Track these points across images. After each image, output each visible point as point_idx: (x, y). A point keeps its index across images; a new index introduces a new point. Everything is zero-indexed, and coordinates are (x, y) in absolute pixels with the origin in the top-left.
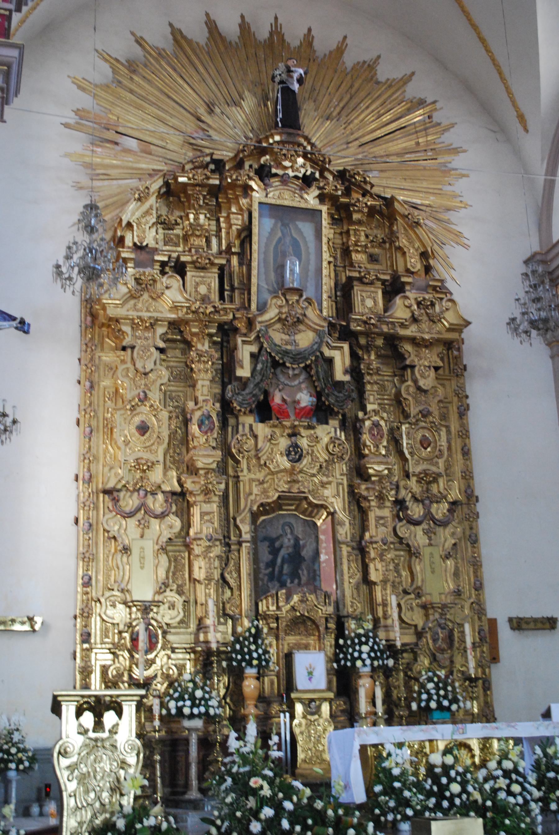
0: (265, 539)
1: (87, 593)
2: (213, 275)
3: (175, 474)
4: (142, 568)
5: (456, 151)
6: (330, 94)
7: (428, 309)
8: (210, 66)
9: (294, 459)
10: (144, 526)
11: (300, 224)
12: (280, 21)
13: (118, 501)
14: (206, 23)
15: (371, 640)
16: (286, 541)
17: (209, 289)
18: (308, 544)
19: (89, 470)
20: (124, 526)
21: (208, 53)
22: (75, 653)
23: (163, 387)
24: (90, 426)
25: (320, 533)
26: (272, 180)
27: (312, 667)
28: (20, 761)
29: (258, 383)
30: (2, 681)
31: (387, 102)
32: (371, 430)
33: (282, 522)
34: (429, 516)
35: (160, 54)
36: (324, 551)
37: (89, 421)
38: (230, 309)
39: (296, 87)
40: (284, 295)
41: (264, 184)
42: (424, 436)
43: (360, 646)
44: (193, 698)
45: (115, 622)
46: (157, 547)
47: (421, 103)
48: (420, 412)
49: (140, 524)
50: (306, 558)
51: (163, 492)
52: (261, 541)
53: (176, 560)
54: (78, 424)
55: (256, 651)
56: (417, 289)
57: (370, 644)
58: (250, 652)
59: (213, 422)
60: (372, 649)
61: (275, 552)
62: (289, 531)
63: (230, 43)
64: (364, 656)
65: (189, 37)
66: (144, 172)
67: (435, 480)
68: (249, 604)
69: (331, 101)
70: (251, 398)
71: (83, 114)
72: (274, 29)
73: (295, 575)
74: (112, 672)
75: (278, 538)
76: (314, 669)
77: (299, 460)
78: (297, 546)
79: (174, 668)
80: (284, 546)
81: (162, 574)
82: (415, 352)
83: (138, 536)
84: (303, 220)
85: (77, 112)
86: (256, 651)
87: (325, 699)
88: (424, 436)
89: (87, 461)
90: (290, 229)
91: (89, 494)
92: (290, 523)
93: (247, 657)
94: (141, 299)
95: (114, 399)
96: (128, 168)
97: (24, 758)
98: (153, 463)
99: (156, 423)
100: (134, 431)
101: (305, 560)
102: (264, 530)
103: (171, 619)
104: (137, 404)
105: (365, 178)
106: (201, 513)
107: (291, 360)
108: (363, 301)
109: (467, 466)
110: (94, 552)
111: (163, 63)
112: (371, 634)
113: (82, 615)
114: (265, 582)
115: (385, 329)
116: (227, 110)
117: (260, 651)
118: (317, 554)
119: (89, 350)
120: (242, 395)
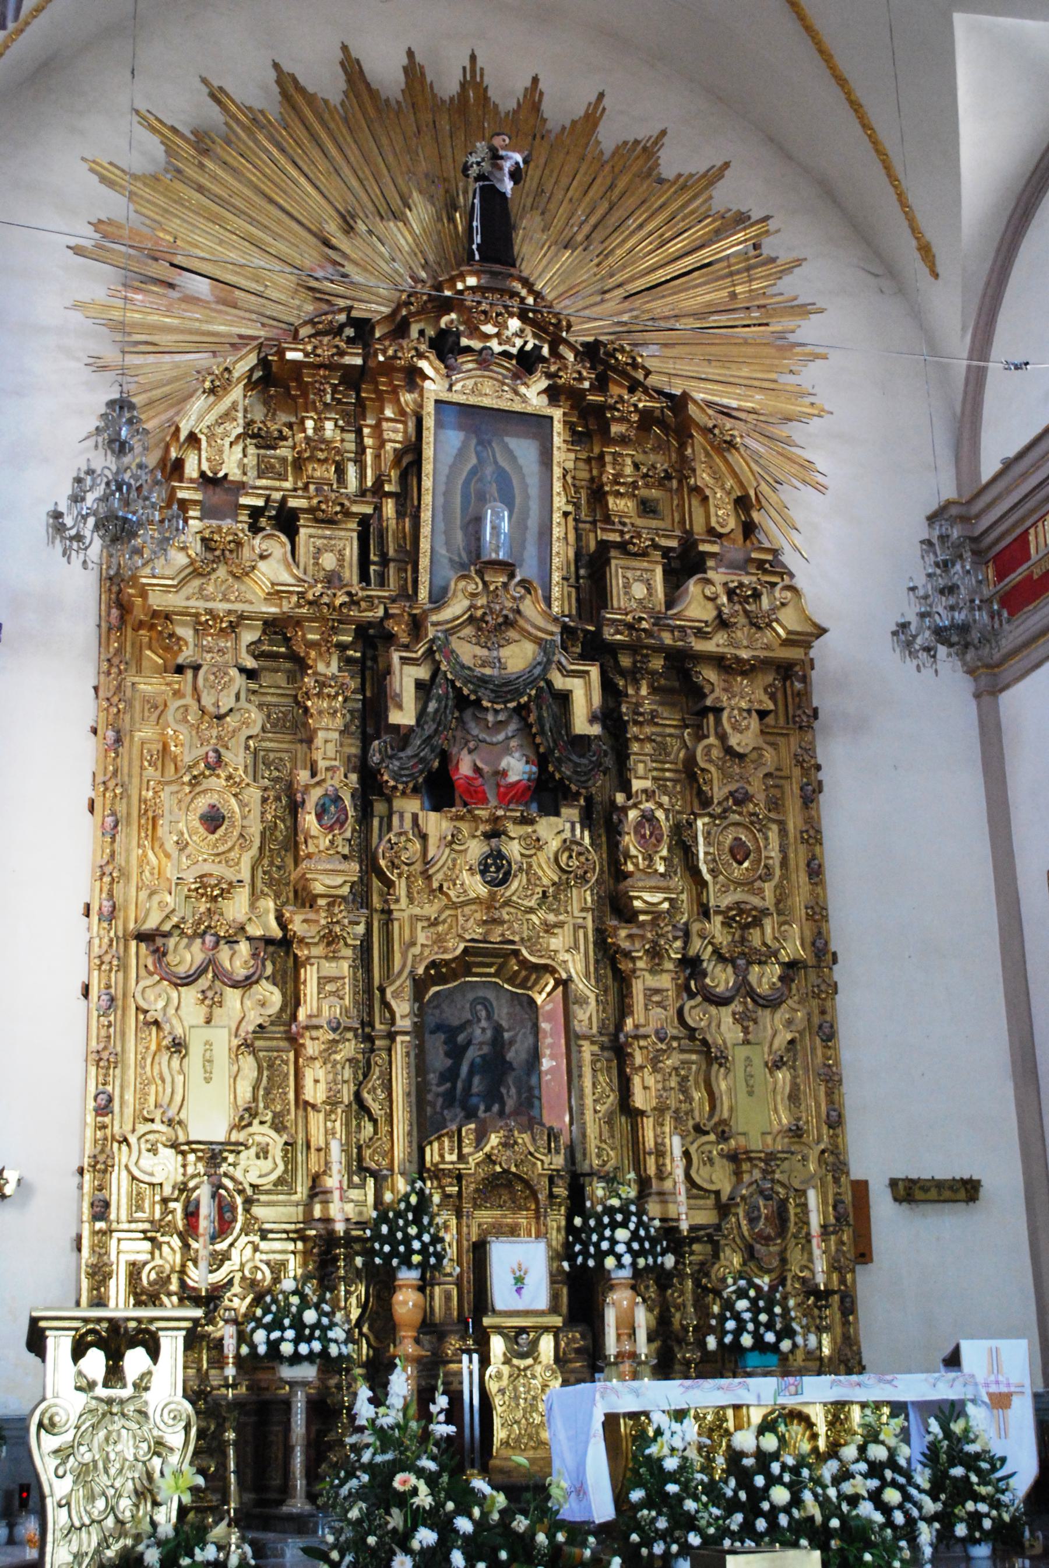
0: (439, 1028)
1: (104, 1127)
4: (208, 1080)
6: (571, 200)
9: (493, 879)
10: (212, 1002)
11: (513, 443)
12: (480, 63)
14: (342, 64)
15: (634, 1219)
17: (341, 560)
18: (519, 1038)
19: (111, 895)
21: (346, 120)
22: (79, 1238)
23: (251, 743)
24: (113, 814)
25: (541, 1019)
27: (523, 1268)
29: (430, 737)
32: (639, 825)
33: (471, 996)
34: (744, 988)
38: (379, 597)
40: (480, 573)
41: (446, 367)
45: (155, 1180)
46: (236, 1042)
47: (741, 220)
48: (731, 794)
50: (515, 1065)
52: (432, 1032)
53: (270, 1066)
54: (92, 809)
56: (727, 567)
57: (632, 1226)
58: (407, 1240)
61: (456, 1052)
62: (483, 1014)
64: (621, 1248)
65: (311, 89)
66: (223, 340)
67: (757, 922)
71: (109, 229)
73: (494, 1096)
74: (147, 1276)
75: (462, 1027)
77: (504, 881)
78: (498, 1043)
81: (245, 1091)
83: (202, 1020)
85: (98, 225)
86: (419, 1237)
87: (546, 1329)
89: (107, 879)
91: (111, 941)
96: (191, 332)
98: (230, 884)
99: (237, 809)
101: (513, 1069)
102: (437, 1012)
105: (634, 359)
106: (319, 978)
110: (119, 1049)
111: (261, 137)
113: (94, 1166)
115: (667, 639)
116: (380, 227)
118: (535, 1057)
119: (114, 670)
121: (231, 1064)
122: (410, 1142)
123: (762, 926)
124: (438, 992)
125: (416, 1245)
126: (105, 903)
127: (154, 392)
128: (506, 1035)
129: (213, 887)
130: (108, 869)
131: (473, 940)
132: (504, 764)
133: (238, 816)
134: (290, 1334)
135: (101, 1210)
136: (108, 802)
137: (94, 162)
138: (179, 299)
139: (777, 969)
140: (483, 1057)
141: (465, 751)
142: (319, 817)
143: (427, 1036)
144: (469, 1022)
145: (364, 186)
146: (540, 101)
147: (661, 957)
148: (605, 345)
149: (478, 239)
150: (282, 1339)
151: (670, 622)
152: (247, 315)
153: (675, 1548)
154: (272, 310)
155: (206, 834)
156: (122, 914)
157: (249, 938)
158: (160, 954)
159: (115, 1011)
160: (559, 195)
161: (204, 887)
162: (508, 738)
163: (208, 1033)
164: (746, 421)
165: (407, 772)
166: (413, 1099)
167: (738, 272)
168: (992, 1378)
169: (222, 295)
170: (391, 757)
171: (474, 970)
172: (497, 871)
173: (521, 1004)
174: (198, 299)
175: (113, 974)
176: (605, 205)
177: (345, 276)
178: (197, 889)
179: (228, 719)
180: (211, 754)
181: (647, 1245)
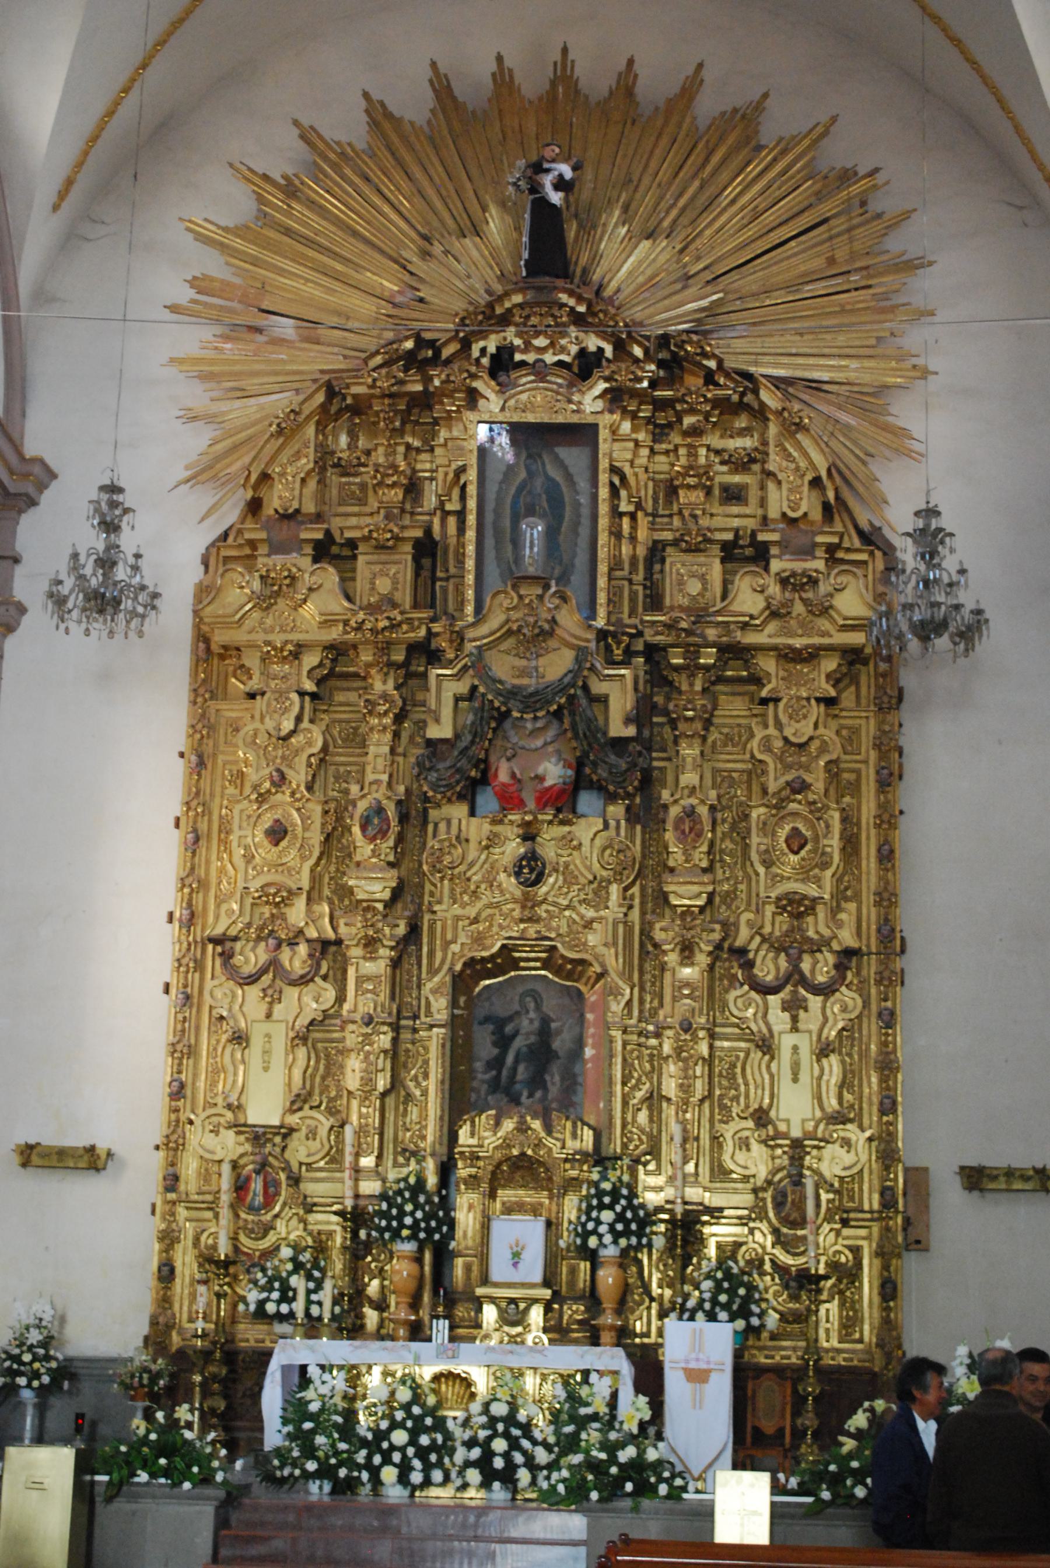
0: (487, 1019)
1: (177, 1110)
2: (404, 557)
3: (327, 909)
4: (266, 1069)
5: (276, 511)
6: (659, 185)
7: (805, 591)
8: (432, 164)
9: (527, 880)
10: (273, 998)
11: (563, 452)
12: (571, 56)
13: (231, 956)
14: (431, 81)
15: (623, 1202)
16: (525, 1023)
17: (395, 582)
18: (566, 1029)
19: (190, 905)
20: (240, 1000)
21: (431, 139)
22: (154, 1206)
23: (313, 760)
24: (195, 830)
25: (587, 1009)
26: (514, 375)
27: (521, 1244)
29: (467, 748)
30: (47, 1248)
31: (775, 186)
32: (679, 821)
33: (520, 989)
34: (795, 977)
35: (343, 154)
36: (590, 1041)
37: (195, 822)
38: (419, 619)
39: (556, 198)
40: (515, 587)
41: (499, 384)
42: (795, 830)
43: (599, 1212)
45: (217, 1158)
46: (292, 1034)
47: (847, 176)
48: (788, 783)
49: (265, 995)
50: (561, 1054)
51: (308, 941)
52: (480, 1023)
53: (328, 1056)
54: (177, 826)
55: (412, 1214)
56: (793, 553)
57: (618, 1208)
58: (402, 1214)
59: (387, 819)
60: (620, 1217)
61: (503, 1042)
62: (532, 1005)
63: (473, 112)
64: (603, 1229)
65: (397, 113)
66: (304, 377)
67: (811, 910)
68: (438, 1134)
69: (662, 198)
70: (452, 776)
71: (203, 284)
72: (559, 73)
73: (537, 1082)
75: (510, 1019)
76: (523, 1248)
77: (538, 880)
78: (545, 1032)
79: (847, 1252)
80: (523, 1031)
82: (782, 673)
83: (262, 1015)
84: (559, 445)
85: (194, 283)
86: (412, 1214)
87: (536, 1301)
88: (795, 830)
89: (186, 890)
90: (543, 464)
91: (189, 945)
92: (533, 990)
93: (394, 1224)
94: (272, 611)
95: (238, 782)
96: (276, 373)
97: (43, 1370)
98: (290, 892)
99: (299, 822)
100: (260, 836)
101: (558, 1058)
102: (487, 1004)
103: (308, 1155)
104: (269, 791)
105: (702, 348)
106: (357, 978)
107: (521, 706)
108: (681, 583)
109: (887, 883)
110: (193, 1041)
111: (348, 171)
112: (625, 1192)
113: (167, 1145)
114: (483, 1093)
115: (711, 633)
116: (456, 245)
117: (419, 1215)
118: (579, 1043)
119: (200, 700)
120: (437, 771)
121: (287, 1054)
122: (442, 1127)
123: (815, 915)
124: (545, 976)
125: (408, 1221)
126: (185, 912)
127: (239, 436)
128: (553, 1025)
129: (275, 895)
130: (187, 882)
131: (510, 938)
132: (540, 770)
133: (299, 829)
134: (275, 1295)
136: (191, 820)
137: (190, 221)
138: (267, 343)
139: (831, 959)
140: (529, 1046)
141: (503, 760)
142: (364, 828)
143: (476, 1027)
144: (517, 1013)
145: (446, 204)
146: (634, 83)
147: (692, 952)
148: (674, 337)
149: (526, 255)
150: (268, 1299)
151: (712, 619)
152: (329, 349)
153: (297, 1472)
154: (353, 340)
155: (270, 846)
156: (200, 922)
157: (308, 941)
158: (227, 957)
159: (191, 1007)
160: (646, 180)
161: (267, 896)
162: (546, 744)
163: (266, 1027)
164: (838, 394)
165: (444, 783)
166: (447, 1086)
167: (839, 235)
168: (693, 1356)
169: (306, 332)
170: (430, 769)
171: (522, 964)
172: (531, 872)
173: (569, 994)
174: (284, 340)
175: (190, 976)
176: (697, 183)
177: (421, 300)
178: (260, 897)
179: (293, 740)
180: (274, 774)
181: (634, 1226)
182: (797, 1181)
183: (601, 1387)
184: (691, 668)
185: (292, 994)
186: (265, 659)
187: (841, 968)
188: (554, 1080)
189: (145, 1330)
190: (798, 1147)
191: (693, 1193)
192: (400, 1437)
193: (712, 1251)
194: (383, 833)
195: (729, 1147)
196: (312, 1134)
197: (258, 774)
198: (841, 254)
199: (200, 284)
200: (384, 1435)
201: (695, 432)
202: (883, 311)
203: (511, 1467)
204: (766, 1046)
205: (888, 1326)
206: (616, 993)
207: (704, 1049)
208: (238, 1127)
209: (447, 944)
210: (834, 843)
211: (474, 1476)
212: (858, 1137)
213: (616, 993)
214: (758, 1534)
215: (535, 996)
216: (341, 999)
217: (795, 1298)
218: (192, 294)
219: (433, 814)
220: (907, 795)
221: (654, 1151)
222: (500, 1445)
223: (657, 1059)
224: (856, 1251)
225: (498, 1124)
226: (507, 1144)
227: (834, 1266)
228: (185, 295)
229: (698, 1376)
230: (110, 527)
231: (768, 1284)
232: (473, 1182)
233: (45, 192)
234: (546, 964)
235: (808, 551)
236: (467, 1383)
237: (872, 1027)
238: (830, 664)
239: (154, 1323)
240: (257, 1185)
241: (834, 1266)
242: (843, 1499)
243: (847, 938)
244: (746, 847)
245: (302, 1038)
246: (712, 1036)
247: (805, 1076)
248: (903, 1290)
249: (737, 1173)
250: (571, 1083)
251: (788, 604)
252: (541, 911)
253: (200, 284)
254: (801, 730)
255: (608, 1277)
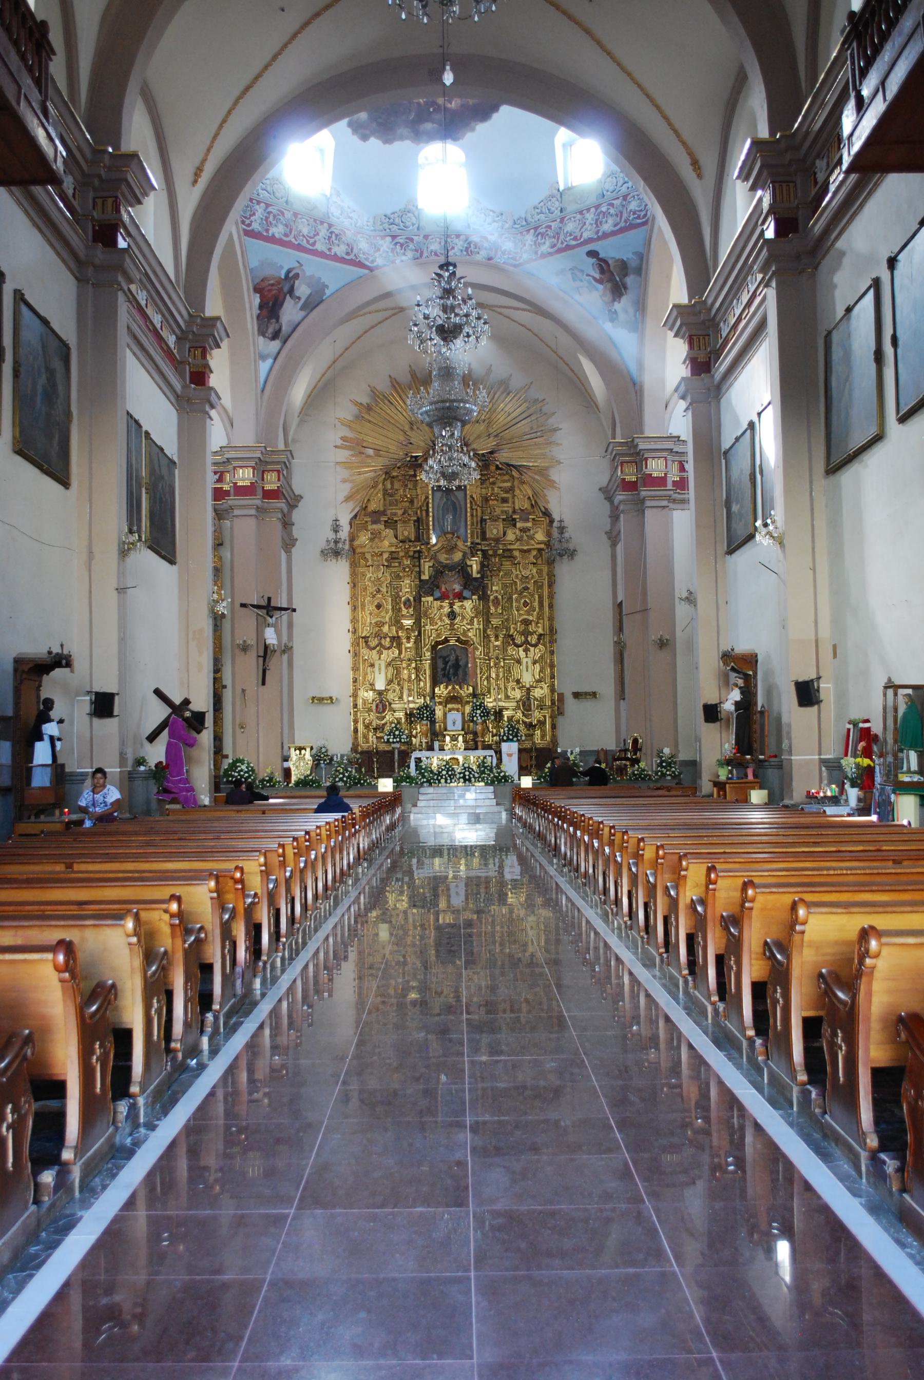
0: (440, 657)
10: (380, 653)
28: (325, 760)
44: (394, 735)
61: (446, 663)
67: (530, 624)
73: (456, 674)
74: (367, 721)
75: (448, 656)
78: (457, 659)
81: (389, 676)
85: (342, 438)
118: (467, 663)
135: (355, 706)
154: (392, 456)
158: (366, 642)
163: (379, 662)
182: (528, 699)
183: (489, 759)
184: (495, 555)
185: (385, 652)
186: (372, 556)
187: (539, 639)
188: (460, 672)
189: (351, 745)
190: (528, 690)
191: (502, 704)
192: (444, 773)
193: (506, 719)
194: (410, 607)
195: (509, 690)
196: (394, 691)
197: (372, 589)
198: (535, 427)
199: (343, 439)
200: (440, 772)
201: (494, 483)
202: (547, 444)
203: (470, 778)
204: (519, 661)
205: (554, 737)
206: (478, 649)
207: (502, 664)
208: (374, 690)
209: (429, 637)
210: (536, 604)
211: (462, 780)
212: (545, 686)
213: (478, 649)
214: (530, 786)
215: (455, 651)
216: (400, 653)
217: (528, 730)
218: (341, 442)
219: (423, 599)
220: (557, 588)
221: (489, 692)
222: (467, 773)
223: (489, 668)
224: (545, 717)
225: (446, 688)
226: (449, 692)
227: (539, 721)
228: (339, 442)
229: (510, 755)
230: (336, 531)
231: (522, 727)
232: (440, 703)
233: (297, 414)
234: (457, 641)
235: (527, 520)
236: (457, 759)
237: (547, 655)
238: (534, 553)
239: (353, 744)
240: (380, 706)
241: (539, 721)
242: (546, 781)
243: (540, 631)
244: (512, 606)
245: (389, 664)
246: (504, 660)
247: (529, 670)
248: (557, 726)
249: (512, 697)
250: (465, 674)
251: (522, 537)
252: (456, 627)
253: (343, 439)
254: (526, 573)
255: (479, 728)
